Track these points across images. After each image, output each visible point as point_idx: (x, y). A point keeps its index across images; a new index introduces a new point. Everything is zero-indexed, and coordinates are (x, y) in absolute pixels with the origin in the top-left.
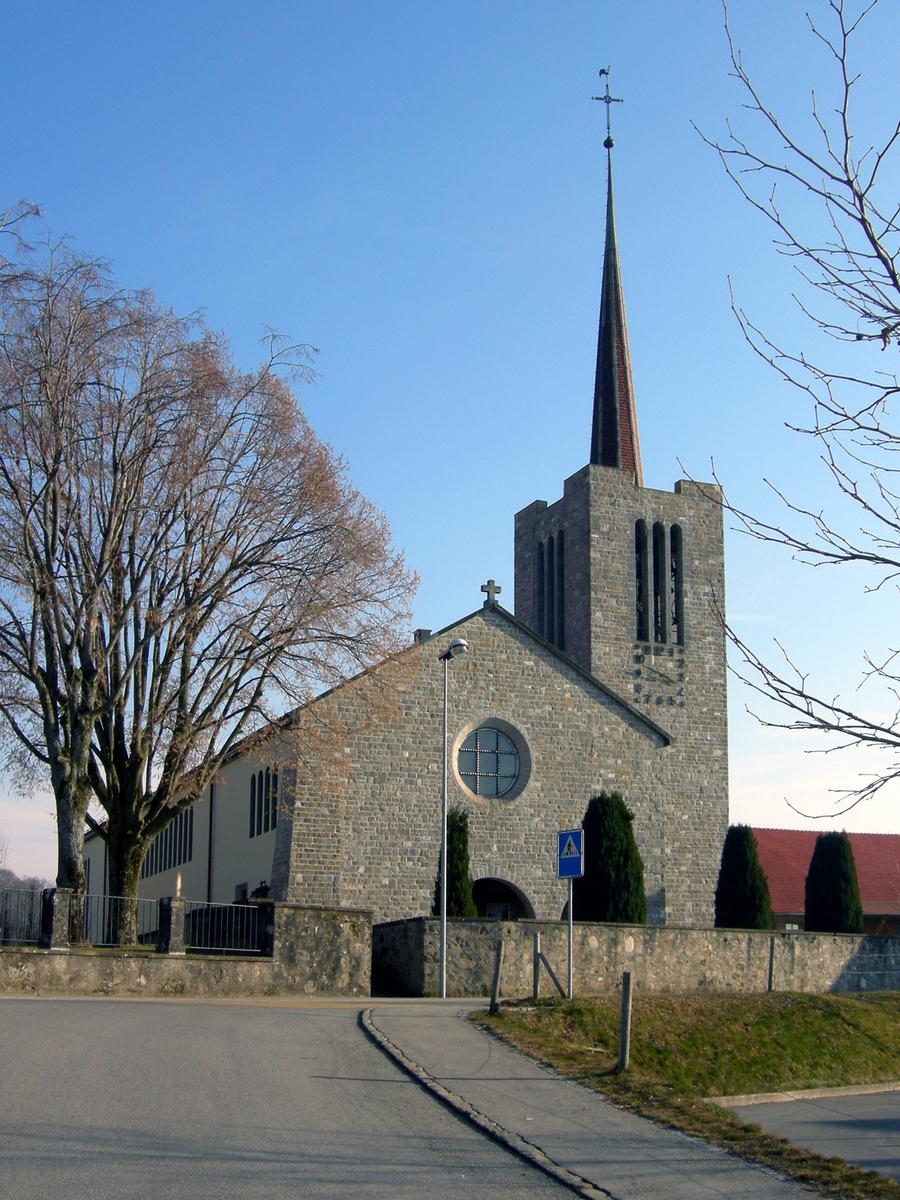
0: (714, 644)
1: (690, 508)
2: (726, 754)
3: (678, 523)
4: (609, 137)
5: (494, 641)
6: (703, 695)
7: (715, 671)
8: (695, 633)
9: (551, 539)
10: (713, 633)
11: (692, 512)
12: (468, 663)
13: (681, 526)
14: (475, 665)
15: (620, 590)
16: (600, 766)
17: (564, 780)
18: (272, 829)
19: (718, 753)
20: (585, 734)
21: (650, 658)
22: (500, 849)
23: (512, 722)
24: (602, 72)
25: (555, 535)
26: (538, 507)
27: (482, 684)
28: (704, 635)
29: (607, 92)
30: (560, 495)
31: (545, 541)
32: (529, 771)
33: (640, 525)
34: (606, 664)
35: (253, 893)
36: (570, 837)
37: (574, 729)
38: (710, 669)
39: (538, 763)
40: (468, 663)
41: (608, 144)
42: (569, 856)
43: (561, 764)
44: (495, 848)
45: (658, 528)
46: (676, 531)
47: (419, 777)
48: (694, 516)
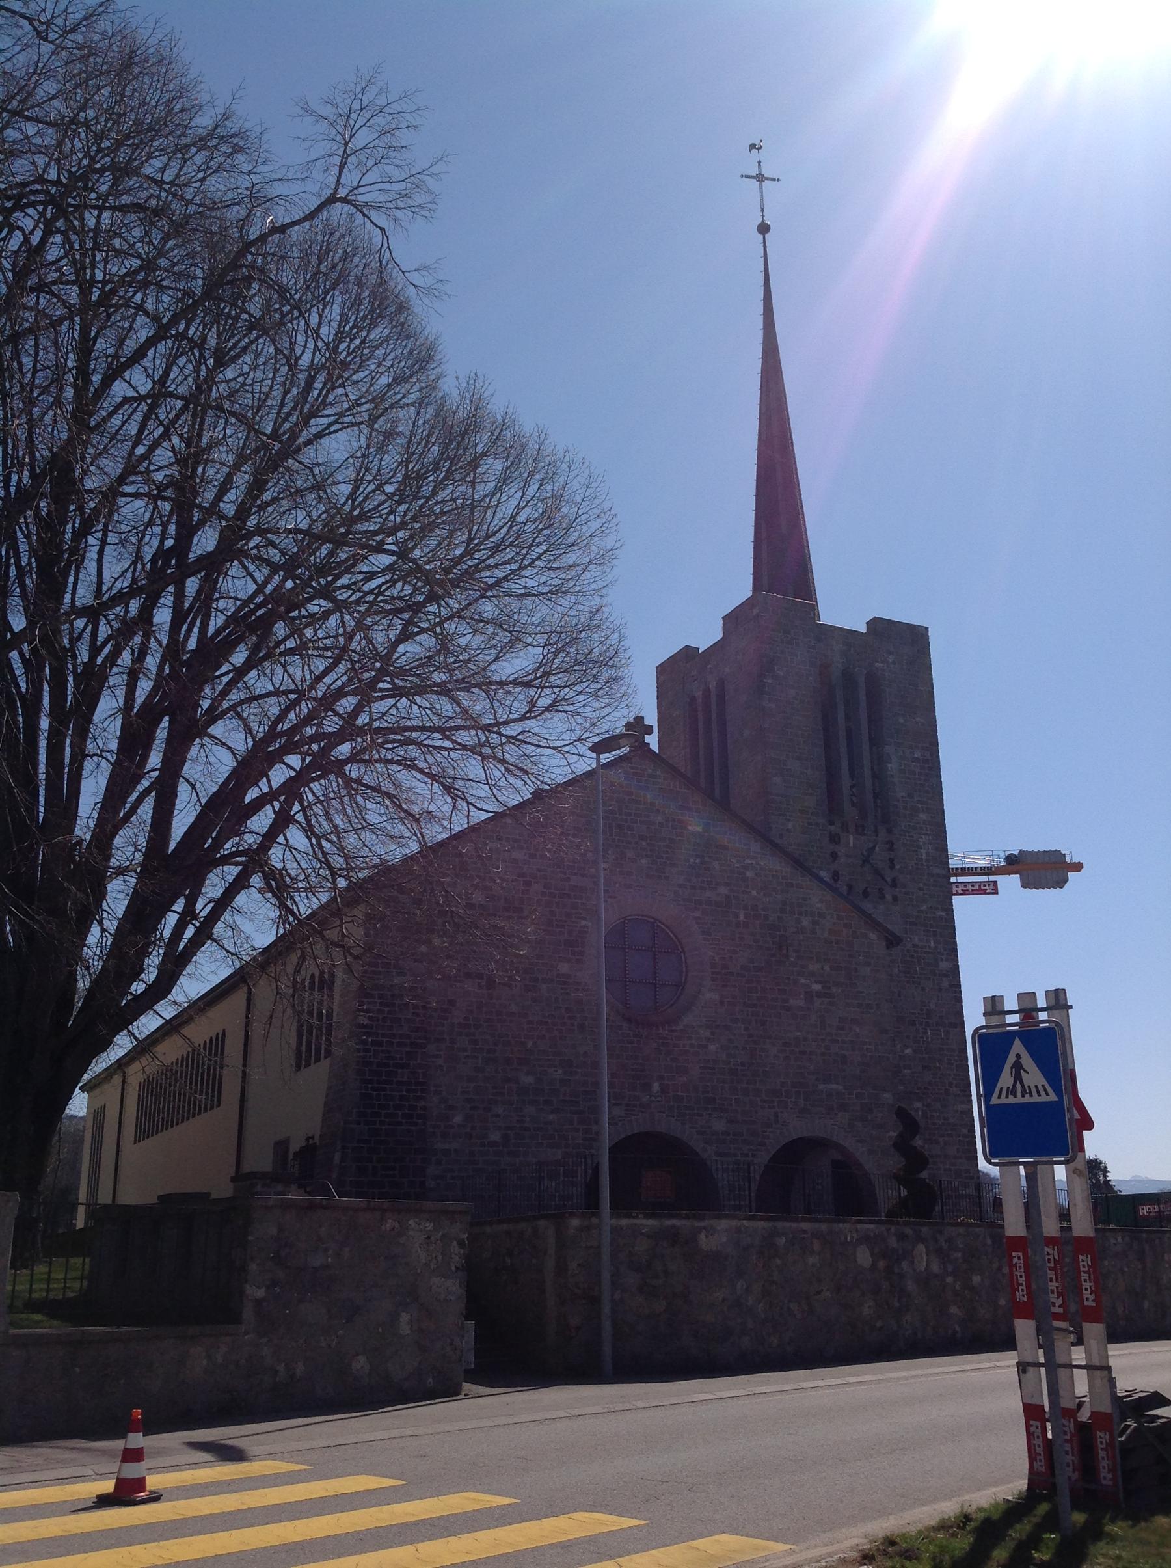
6: (920, 889)
9: (707, 692)
18: (326, 1057)
19: (944, 965)
24: (753, 146)
25: (713, 685)
26: (688, 653)
29: (761, 188)
30: (716, 634)
31: (699, 694)
35: (296, 1154)
36: (1017, 1042)
38: (927, 854)
41: (764, 229)
42: (1019, 1099)
44: (656, 1086)
48: (894, 663)
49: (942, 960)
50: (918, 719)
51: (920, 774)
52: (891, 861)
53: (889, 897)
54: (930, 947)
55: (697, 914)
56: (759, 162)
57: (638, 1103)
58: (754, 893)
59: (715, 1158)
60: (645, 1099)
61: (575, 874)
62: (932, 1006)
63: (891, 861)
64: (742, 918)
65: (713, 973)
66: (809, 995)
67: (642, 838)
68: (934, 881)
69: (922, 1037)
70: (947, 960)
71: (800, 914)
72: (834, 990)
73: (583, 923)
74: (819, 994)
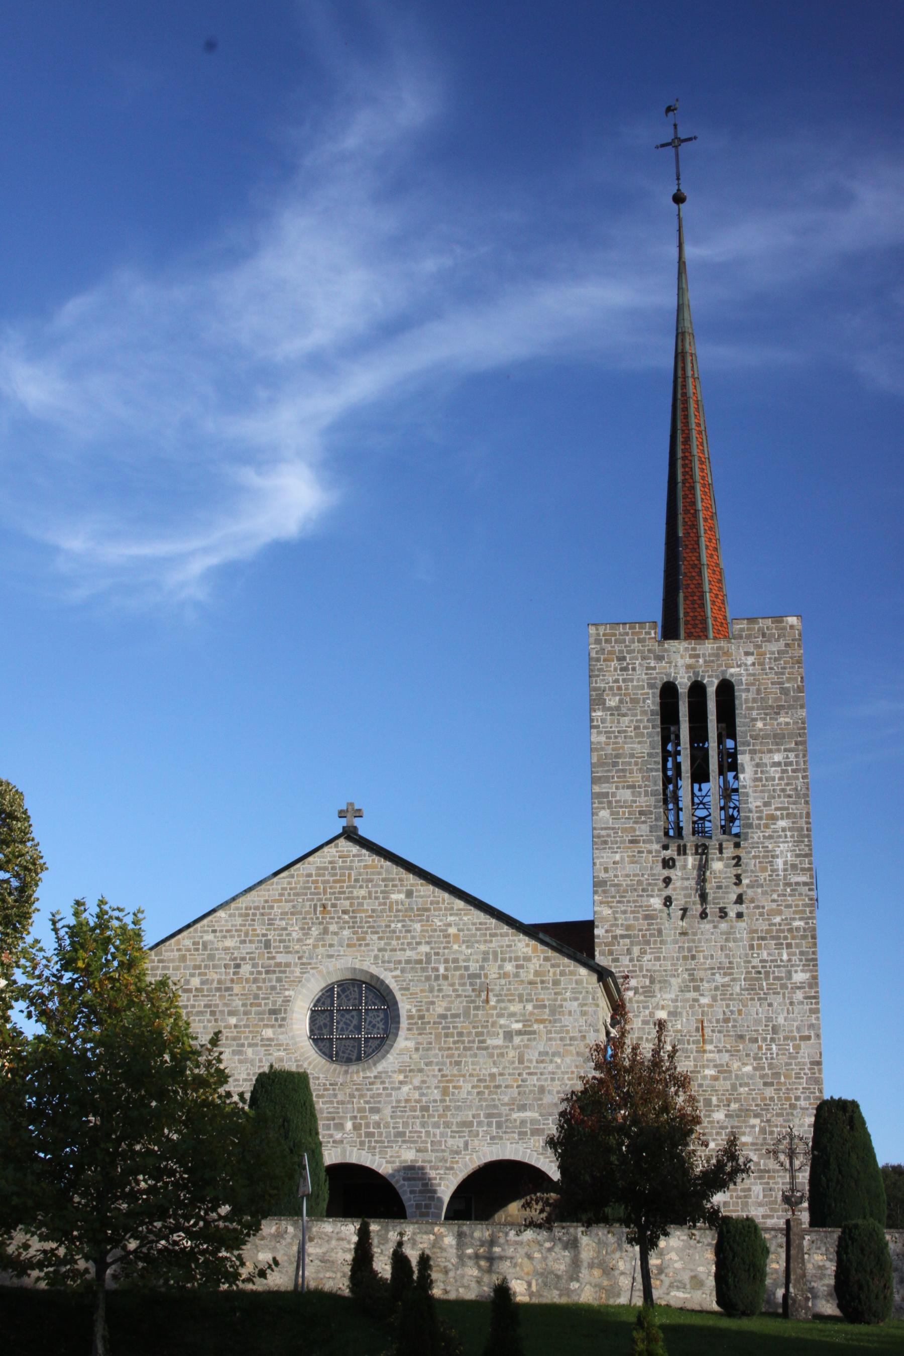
0: (790, 829)
1: (747, 654)
2: (815, 978)
3: (728, 677)
4: (679, 190)
5: (350, 875)
6: (773, 901)
7: (794, 867)
8: (760, 818)
10: (788, 814)
11: (750, 660)
12: (315, 905)
13: (733, 680)
14: (324, 906)
15: (637, 777)
16: (500, 1015)
17: (447, 1035)
20: (478, 976)
21: (685, 861)
22: (356, 1127)
23: (374, 970)
24: (669, 109)
27: (333, 928)
28: (773, 818)
32: (398, 1029)
33: (668, 691)
34: (616, 876)
37: (462, 972)
38: (785, 863)
39: (410, 1017)
40: (315, 905)
43: (444, 1017)
44: (349, 1125)
45: (697, 689)
46: (726, 689)
47: (250, 1045)
48: (753, 664)
49: (796, 972)
50: (782, 720)
51: (781, 779)
52: (738, 877)
53: (732, 914)
54: (782, 961)
55: (398, 973)
56: (675, 125)
57: (331, 1140)
58: (456, 947)
59: (402, 1182)
60: (338, 1136)
61: (281, 952)
62: (781, 1020)
63: (738, 877)
64: (442, 970)
65: (409, 1024)
66: (509, 1035)
67: (345, 912)
68: (791, 890)
69: (766, 1054)
70: (802, 971)
71: (503, 960)
72: (535, 1027)
73: (287, 993)
74: (519, 1033)
